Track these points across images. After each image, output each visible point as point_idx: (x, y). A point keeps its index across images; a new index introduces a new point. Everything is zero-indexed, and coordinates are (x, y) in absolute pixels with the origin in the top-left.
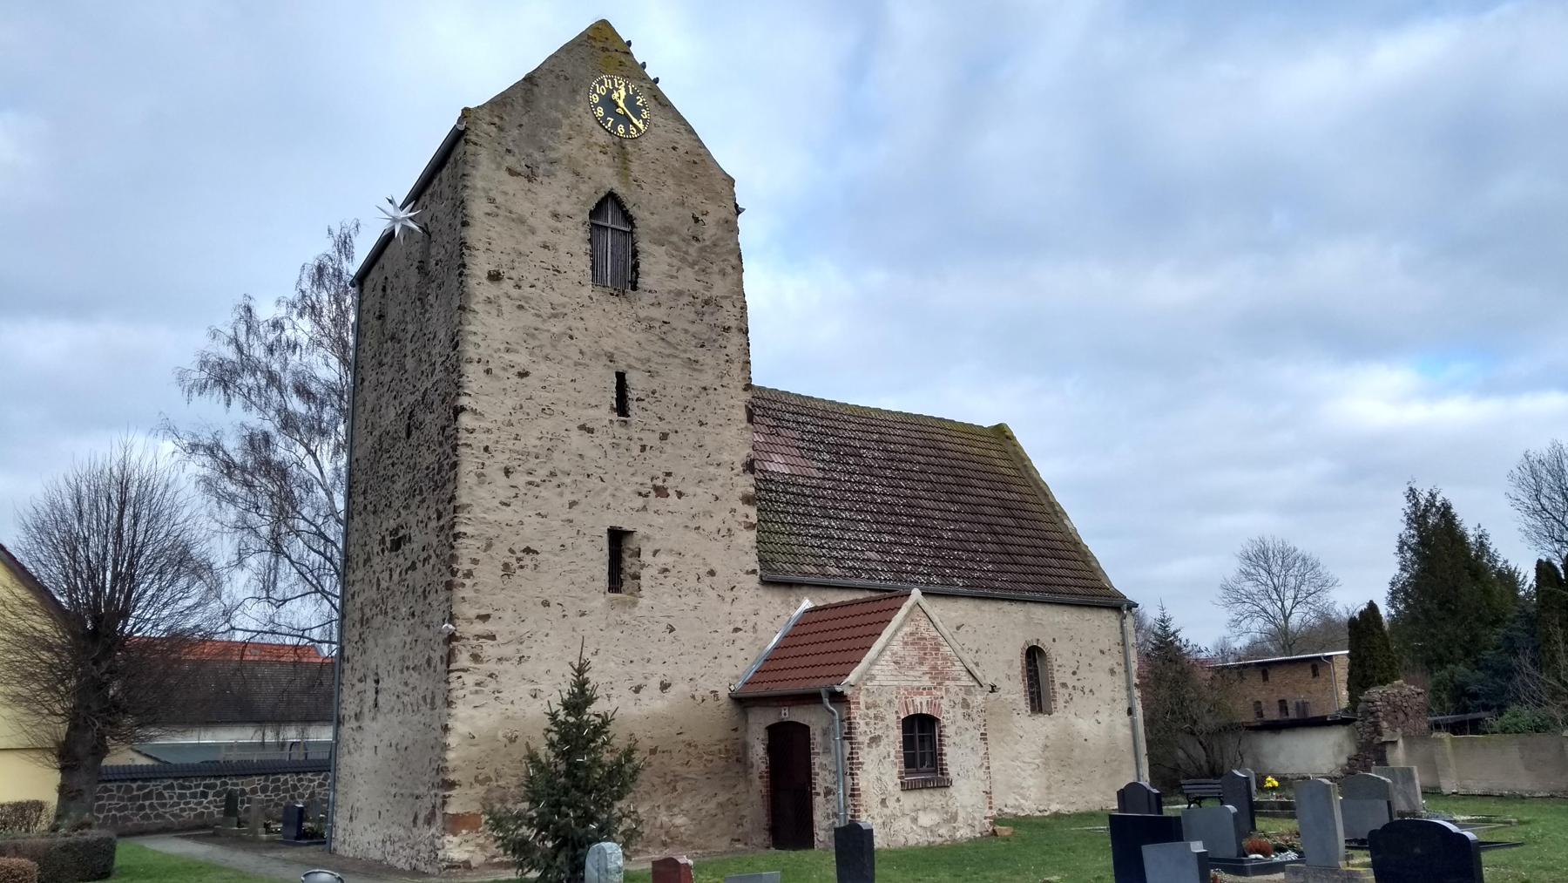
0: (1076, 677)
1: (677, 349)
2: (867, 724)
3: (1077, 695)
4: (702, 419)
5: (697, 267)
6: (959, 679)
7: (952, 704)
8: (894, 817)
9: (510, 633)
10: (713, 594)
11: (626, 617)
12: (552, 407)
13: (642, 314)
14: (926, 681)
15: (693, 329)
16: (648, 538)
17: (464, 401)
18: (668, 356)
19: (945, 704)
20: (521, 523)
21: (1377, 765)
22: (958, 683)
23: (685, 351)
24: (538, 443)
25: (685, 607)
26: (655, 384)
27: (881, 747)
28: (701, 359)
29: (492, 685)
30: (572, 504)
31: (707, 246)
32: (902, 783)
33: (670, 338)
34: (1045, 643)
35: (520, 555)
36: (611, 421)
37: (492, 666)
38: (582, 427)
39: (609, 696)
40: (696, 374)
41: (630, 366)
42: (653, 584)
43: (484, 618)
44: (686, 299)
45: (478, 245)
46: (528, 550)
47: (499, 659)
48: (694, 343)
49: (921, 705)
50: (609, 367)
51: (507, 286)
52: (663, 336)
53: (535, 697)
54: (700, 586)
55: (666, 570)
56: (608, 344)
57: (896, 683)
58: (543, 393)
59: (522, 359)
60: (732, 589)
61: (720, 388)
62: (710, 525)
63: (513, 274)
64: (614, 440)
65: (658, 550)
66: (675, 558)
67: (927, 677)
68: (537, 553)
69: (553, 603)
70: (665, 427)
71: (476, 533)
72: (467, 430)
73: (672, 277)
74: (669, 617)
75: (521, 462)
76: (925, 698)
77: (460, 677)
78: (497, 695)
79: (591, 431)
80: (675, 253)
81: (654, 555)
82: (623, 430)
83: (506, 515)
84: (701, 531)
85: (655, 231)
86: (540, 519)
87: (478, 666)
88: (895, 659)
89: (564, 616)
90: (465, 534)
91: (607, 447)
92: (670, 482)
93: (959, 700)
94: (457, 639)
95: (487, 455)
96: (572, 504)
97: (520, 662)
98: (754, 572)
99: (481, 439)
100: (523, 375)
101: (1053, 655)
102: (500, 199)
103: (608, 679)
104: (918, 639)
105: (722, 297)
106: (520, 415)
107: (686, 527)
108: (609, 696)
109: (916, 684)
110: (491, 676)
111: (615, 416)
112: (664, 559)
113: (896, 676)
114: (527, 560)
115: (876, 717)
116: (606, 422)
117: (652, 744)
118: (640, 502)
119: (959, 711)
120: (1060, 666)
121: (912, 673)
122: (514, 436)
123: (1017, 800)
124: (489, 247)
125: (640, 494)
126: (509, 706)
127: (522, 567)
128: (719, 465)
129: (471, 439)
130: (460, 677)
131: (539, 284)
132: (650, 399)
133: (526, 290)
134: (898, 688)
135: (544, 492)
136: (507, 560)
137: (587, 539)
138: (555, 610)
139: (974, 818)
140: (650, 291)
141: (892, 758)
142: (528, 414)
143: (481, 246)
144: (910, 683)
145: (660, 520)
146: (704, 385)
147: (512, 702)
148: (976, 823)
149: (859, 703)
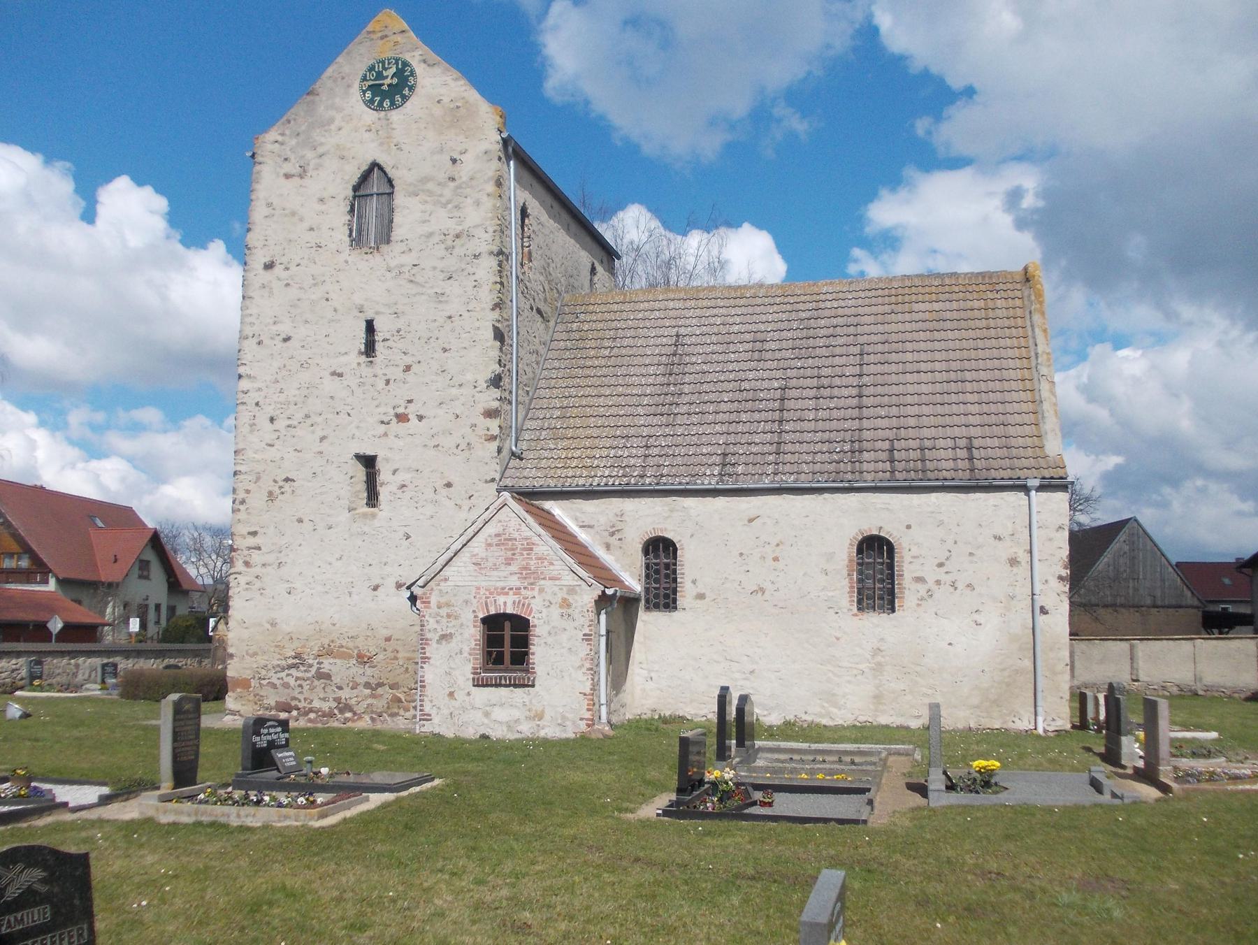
1: (424, 286)
2: (437, 622)
4: (445, 346)
5: (450, 206)
6: (559, 579)
7: (548, 604)
8: (464, 709)
9: (273, 544)
10: (450, 504)
11: (366, 529)
12: (309, 361)
13: (393, 263)
14: (514, 582)
15: (440, 265)
16: (387, 460)
17: (242, 370)
18: (415, 295)
19: (536, 604)
20: (282, 458)
22: (557, 582)
23: (432, 287)
24: (297, 392)
25: (421, 517)
26: (400, 323)
28: (448, 292)
29: (258, 584)
30: (322, 439)
31: (464, 182)
32: (473, 679)
33: (419, 279)
35: (281, 483)
36: (359, 364)
37: (257, 570)
38: (334, 374)
39: (350, 593)
40: (440, 306)
41: (377, 313)
42: (392, 499)
43: (254, 534)
44: (436, 239)
45: (256, 244)
46: (287, 480)
47: (264, 565)
48: (441, 277)
49: (507, 605)
50: (358, 317)
51: (278, 270)
52: (412, 278)
53: (289, 593)
54: (437, 497)
55: (404, 486)
56: (358, 299)
58: (303, 351)
59: (285, 328)
60: (470, 498)
61: (466, 314)
62: (448, 442)
63: (284, 260)
64: (361, 380)
65: (398, 469)
66: (414, 474)
67: (515, 577)
68: (294, 481)
69: (306, 520)
70: (408, 360)
71: (248, 470)
72: (243, 392)
73: (424, 222)
74: (405, 526)
75: (282, 411)
76: (510, 599)
77: (236, 578)
78: (262, 591)
79: (340, 375)
80: (428, 199)
81: (394, 474)
82: (370, 370)
83: (272, 453)
84: (439, 448)
85: (410, 184)
86: (296, 454)
87: (249, 570)
88: (474, 561)
89: (315, 530)
90: (240, 471)
91: (354, 387)
92: (412, 408)
94: (234, 550)
95: (257, 408)
96: (322, 439)
97: (279, 567)
98: (493, 480)
99: (254, 397)
100: (287, 339)
102: (276, 202)
103: (351, 580)
104: (505, 540)
105: (474, 227)
106: (284, 372)
107: (425, 446)
108: (350, 593)
109: (501, 584)
110: (257, 577)
111: (363, 358)
112: (402, 477)
114: (287, 486)
115: (449, 616)
116: (355, 365)
117: (386, 633)
118: (383, 428)
119: (556, 611)
120: (914, 557)
121: (495, 573)
122: (279, 390)
123: (823, 707)
124: (266, 243)
125: (382, 422)
126: (271, 600)
127: (283, 493)
128: (460, 385)
129: (246, 398)
130: (236, 578)
131: (304, 262)
132: (395, 338)
133: (293, 269)
134: (478, 588)
135: (299, 432)
136: (270, 489)
137: (334, 466)
138: (307, 526)
139: (564, 718)
140: (402, 241)
141: (466, 654)
142: (290, 371)
143: (259, 244)
144: (491, 583)
145: (401, 443)
146: (449, 314)
147: (273, 597)
148: (568, 723)
149: (429, 602)
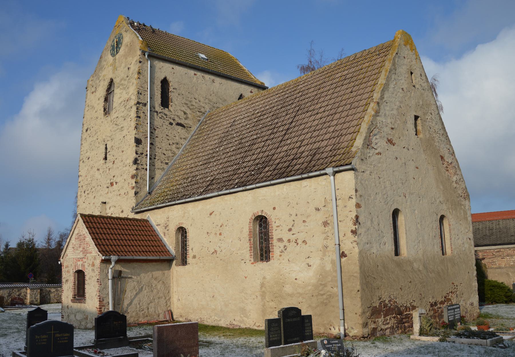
0: (292, 232)
3: (291, 247)
21: (376, 307)
27: (68, 284)
34: (268, 213)
57: (73, 257)
93: (91, 263)
101: (273, 220)
113: (73, 254)
120: (278, 226)
